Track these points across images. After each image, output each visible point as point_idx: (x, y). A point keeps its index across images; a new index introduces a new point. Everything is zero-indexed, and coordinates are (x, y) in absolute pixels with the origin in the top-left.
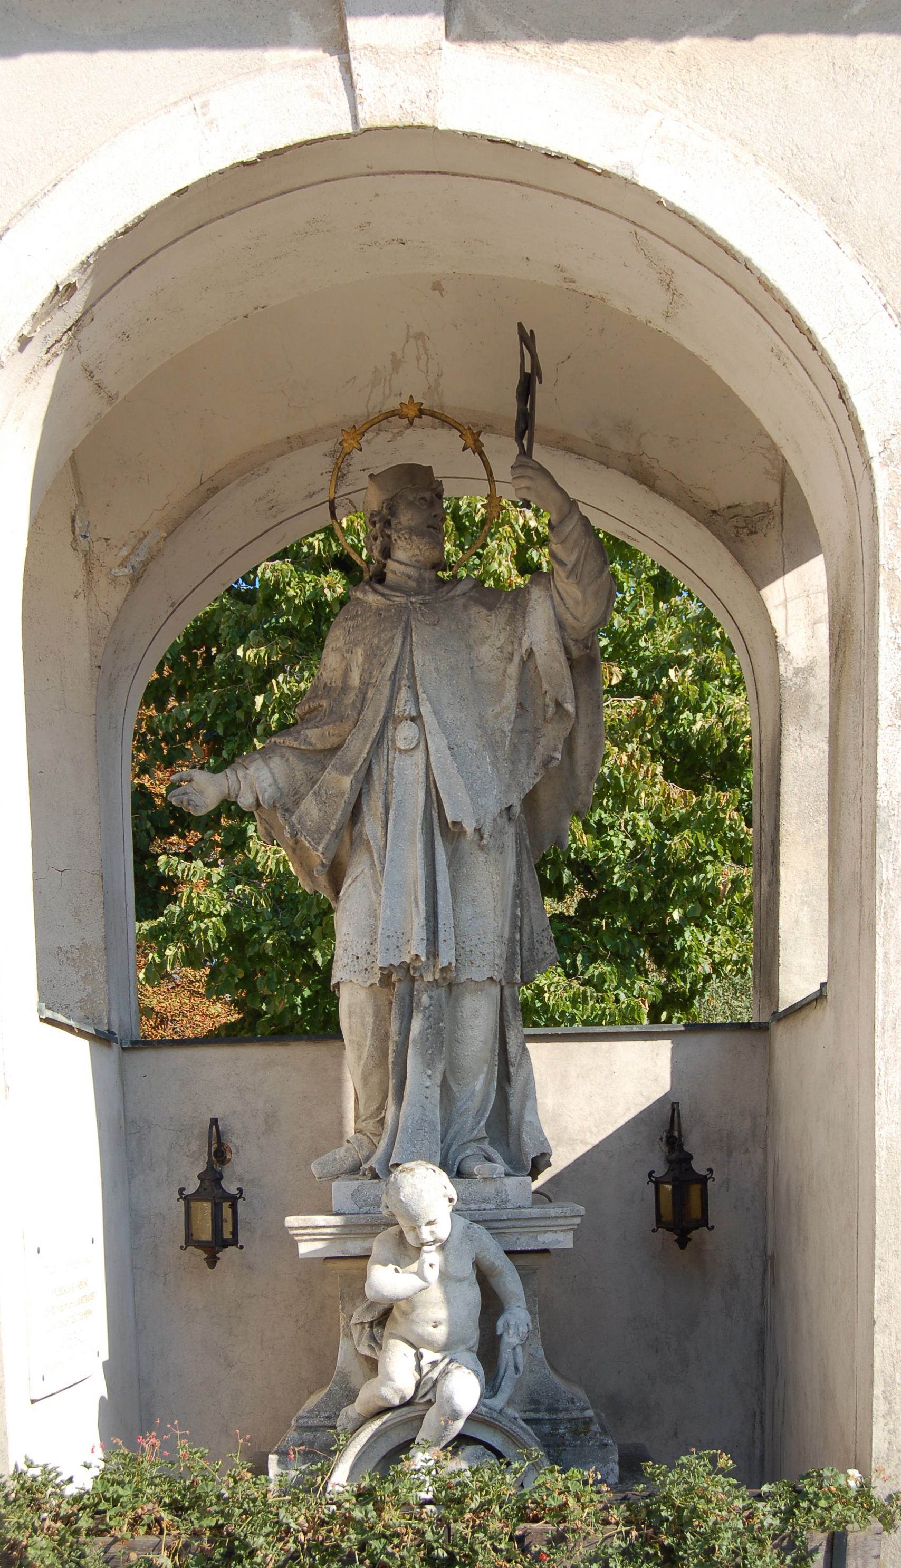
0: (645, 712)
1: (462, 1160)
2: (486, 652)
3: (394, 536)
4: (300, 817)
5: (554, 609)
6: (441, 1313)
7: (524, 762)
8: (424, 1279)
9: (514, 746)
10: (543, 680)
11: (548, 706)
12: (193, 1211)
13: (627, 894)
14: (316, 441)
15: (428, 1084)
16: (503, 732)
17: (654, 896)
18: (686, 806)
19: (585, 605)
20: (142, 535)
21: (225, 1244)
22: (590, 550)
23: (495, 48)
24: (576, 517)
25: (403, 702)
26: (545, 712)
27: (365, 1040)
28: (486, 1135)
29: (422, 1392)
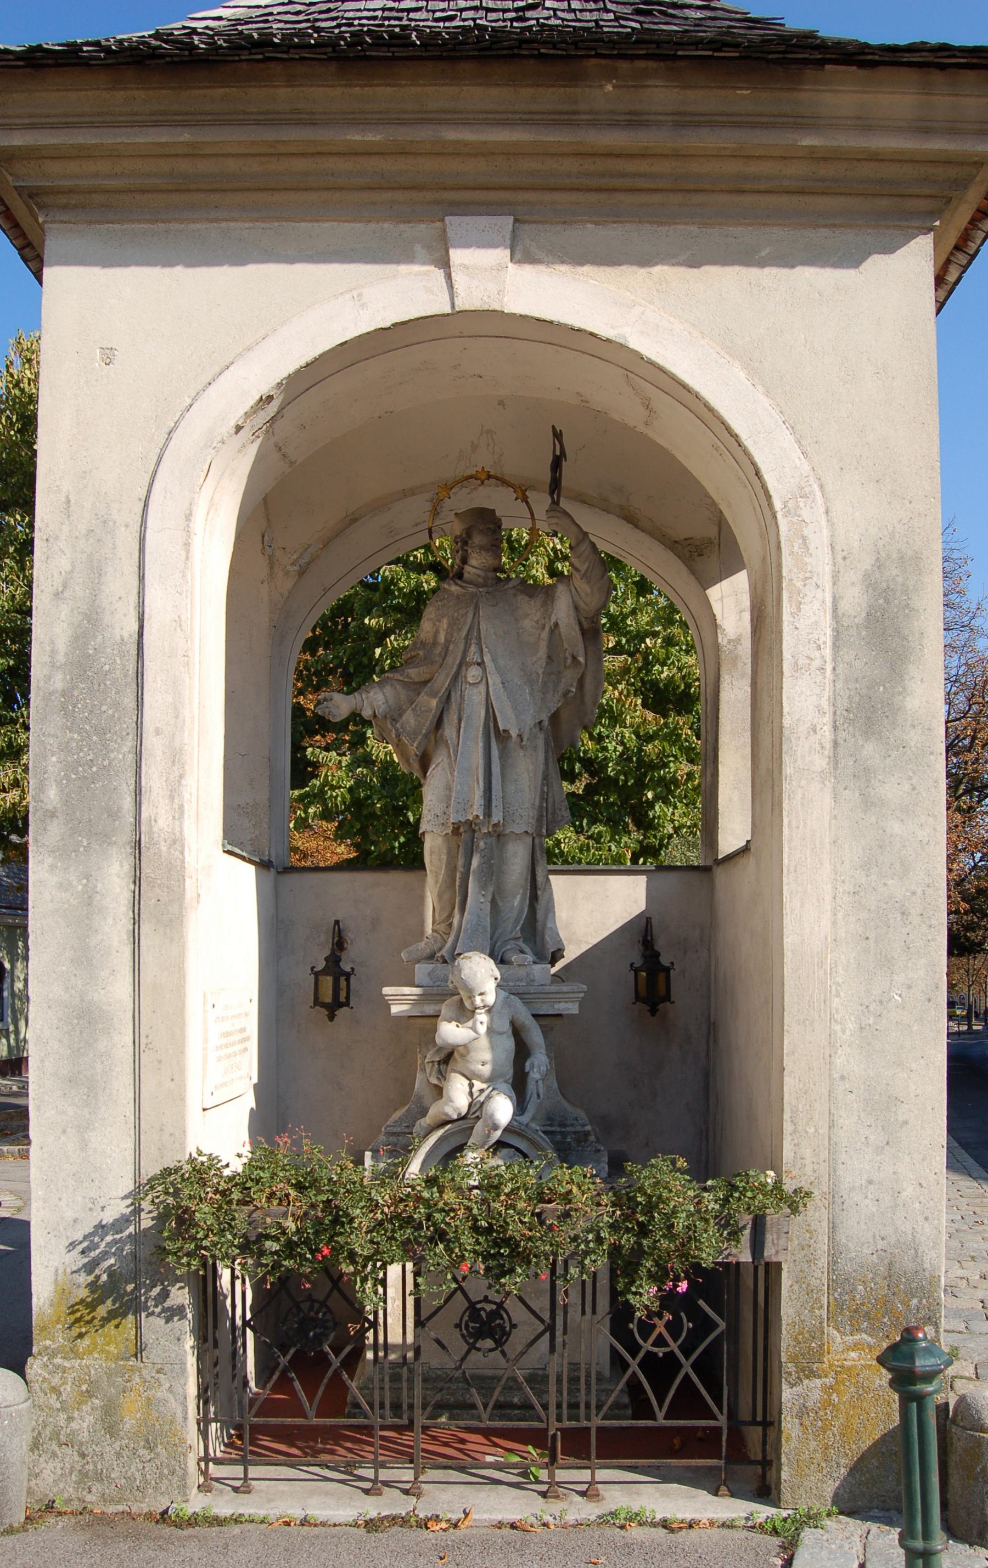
2: (527, 623)
3: (470, 551)
6: (487, 1056)
8: (476, 1032)
9: (545, 683)
13: (617, 780)
21: (341, 1005)
23: (541, 268)
26: (565, 661)
29: (473, 1110)
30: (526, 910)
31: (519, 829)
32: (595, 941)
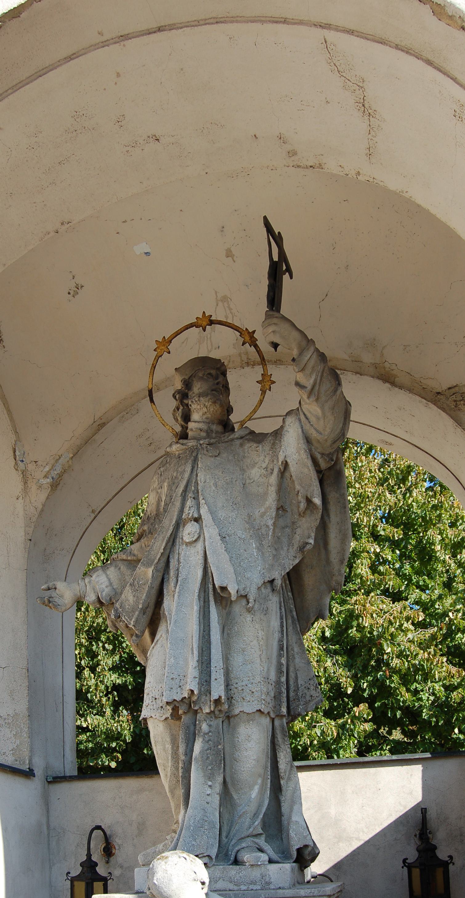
0: (436, 633)
1: (238, 851)
2: (255, 473)
4: (122, 603)
5: (302, 428)
7: (285, 549)
10: (296, 483)
11: (301, 502)
12: (76, 887)
13: (431, 722)
14: (166, 387)
15: (208, 792)
16: (268, 526)
17: (445, 723)
18: (459, 677)
19: (324, 419)
20: (58, 457)
22: (325, 374)
24: (312, 349)
25: (188, 508)
27: (168, 762)
28: (261, 831)
30: (266, 802)
31: (250, 708)
32: (366, 837)
